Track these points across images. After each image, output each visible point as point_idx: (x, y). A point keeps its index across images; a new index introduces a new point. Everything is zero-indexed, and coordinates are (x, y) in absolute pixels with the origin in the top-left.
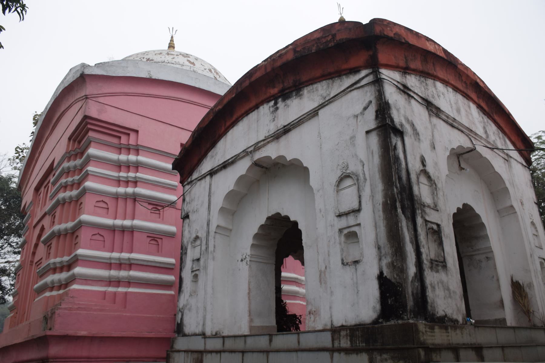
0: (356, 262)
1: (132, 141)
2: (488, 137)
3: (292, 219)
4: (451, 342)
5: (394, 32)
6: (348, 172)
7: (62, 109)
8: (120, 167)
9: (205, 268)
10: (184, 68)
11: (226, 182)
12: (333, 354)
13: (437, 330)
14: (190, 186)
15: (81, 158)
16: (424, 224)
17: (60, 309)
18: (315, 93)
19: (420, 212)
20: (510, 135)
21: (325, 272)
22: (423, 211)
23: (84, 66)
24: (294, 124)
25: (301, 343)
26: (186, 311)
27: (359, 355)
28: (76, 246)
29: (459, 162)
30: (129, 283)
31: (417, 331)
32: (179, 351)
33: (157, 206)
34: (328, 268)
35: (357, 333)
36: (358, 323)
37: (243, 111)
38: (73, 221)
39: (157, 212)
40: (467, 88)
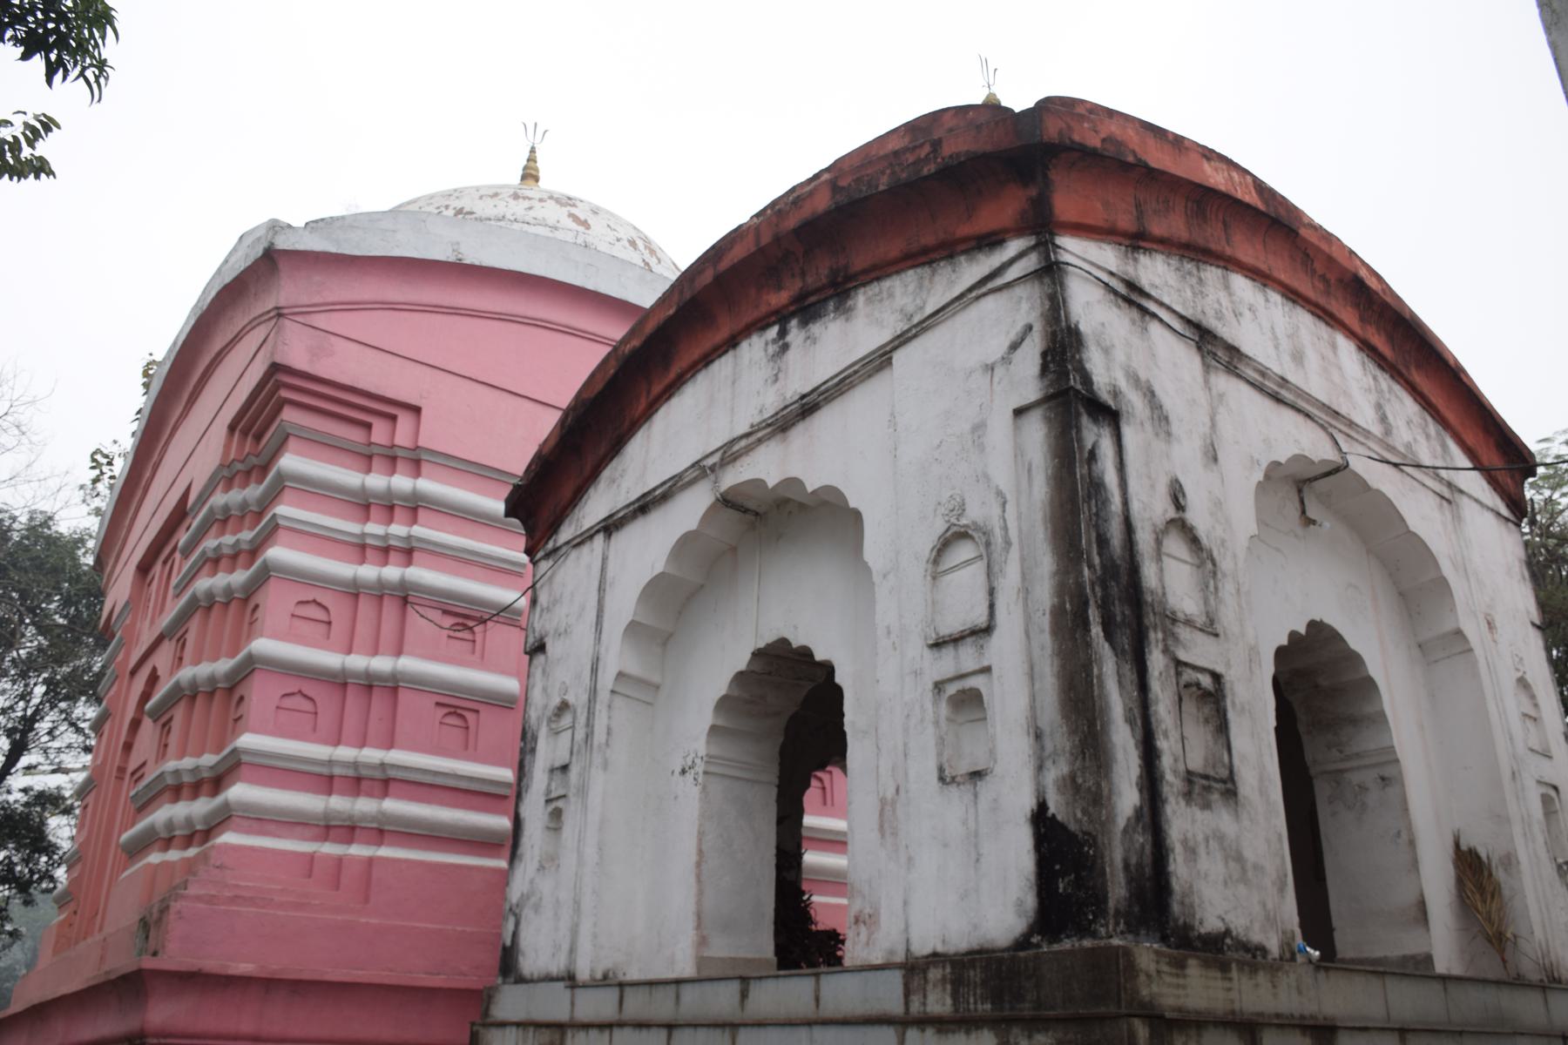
0: (977, 775)
1: (403, 436)
2: (1388, 432)
3: (819, 656)
4: (1237, 1006)
5: (1103, 135)
6: (964, 521)
7: (218, 344)
8: (367, 507)
9: (583, 791)
10: (559, 235)
11: (647, 550)
12: (904, 1034)
13: (1194, 969)
14: (551, 562)
15: (260, 482)
16: (1172, 672)
17: (183, 897)
18: (886, 303)
19: (1160, 635)
20: (1459, 428)
21: (894, 802)
22: (1170, 635)
23: (275, 226)
24: (827, 391)
25: (822, 1002)
26: (527, 913)
27: (973, 1036)
28: (237, 724)
29: (1302, 502)
30: (381, 832)
31: (1131, 969)
32: (503, 1025)
33: (467, 619)
34: (902, 791)
35: (972, 973)
36: (975, 946)
37: (696, 353)
38: (233, 656)
39: (466, 635)
40: (1327, 293)
